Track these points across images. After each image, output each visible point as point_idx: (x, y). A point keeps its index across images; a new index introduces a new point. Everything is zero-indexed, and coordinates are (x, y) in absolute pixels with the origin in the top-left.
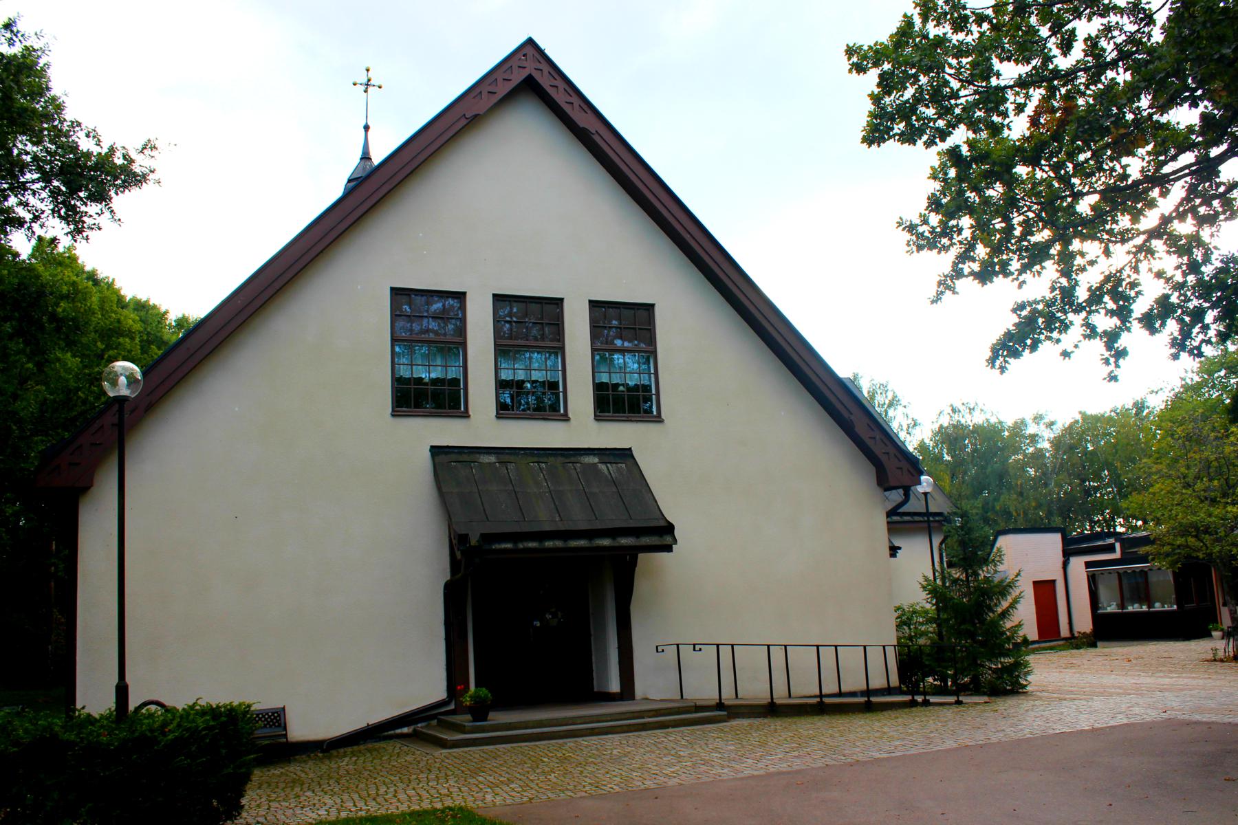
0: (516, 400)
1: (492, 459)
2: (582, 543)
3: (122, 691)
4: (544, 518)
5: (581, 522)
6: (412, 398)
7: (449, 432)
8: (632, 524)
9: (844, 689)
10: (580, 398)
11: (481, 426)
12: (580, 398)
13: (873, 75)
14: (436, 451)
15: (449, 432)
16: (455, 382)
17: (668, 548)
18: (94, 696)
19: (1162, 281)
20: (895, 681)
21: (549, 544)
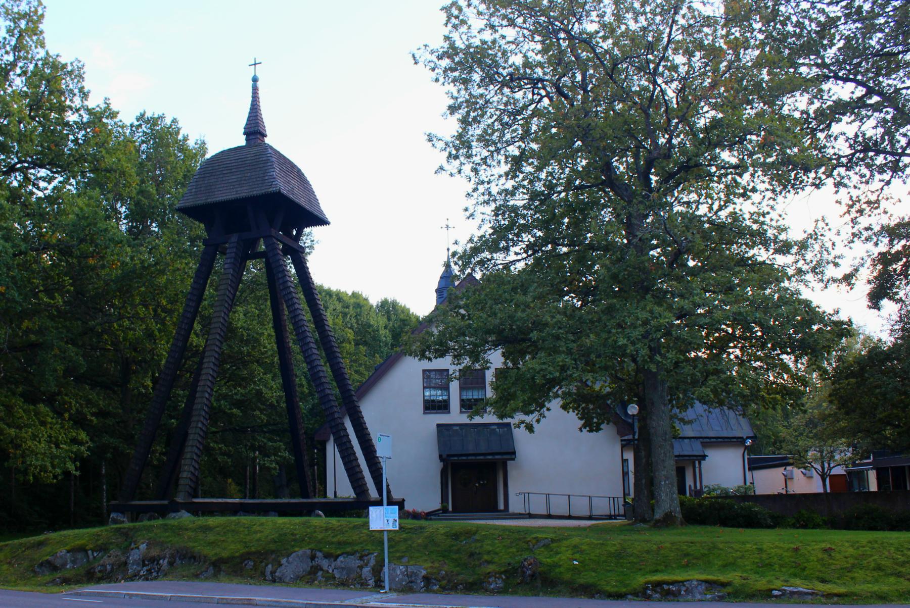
0: (466, 405)
1: (458, 428)
2: (482, 457)
3: (335, 493)
4: (471, 449)
5: (496, 449)
6: (431, 406)
7: (443, 419)
8: (502, 451)
9: (595, 513)
10: (455, 404)
11: (456, 416)
12: (455, 404)
13: (458, 116)
14: (438, 425)
15: (443, 419)
16: (445, 401)
17: (513, 459)
18: (330, 494)
19: (832, 312)
20: (622, 512)
21: (470, 458)
